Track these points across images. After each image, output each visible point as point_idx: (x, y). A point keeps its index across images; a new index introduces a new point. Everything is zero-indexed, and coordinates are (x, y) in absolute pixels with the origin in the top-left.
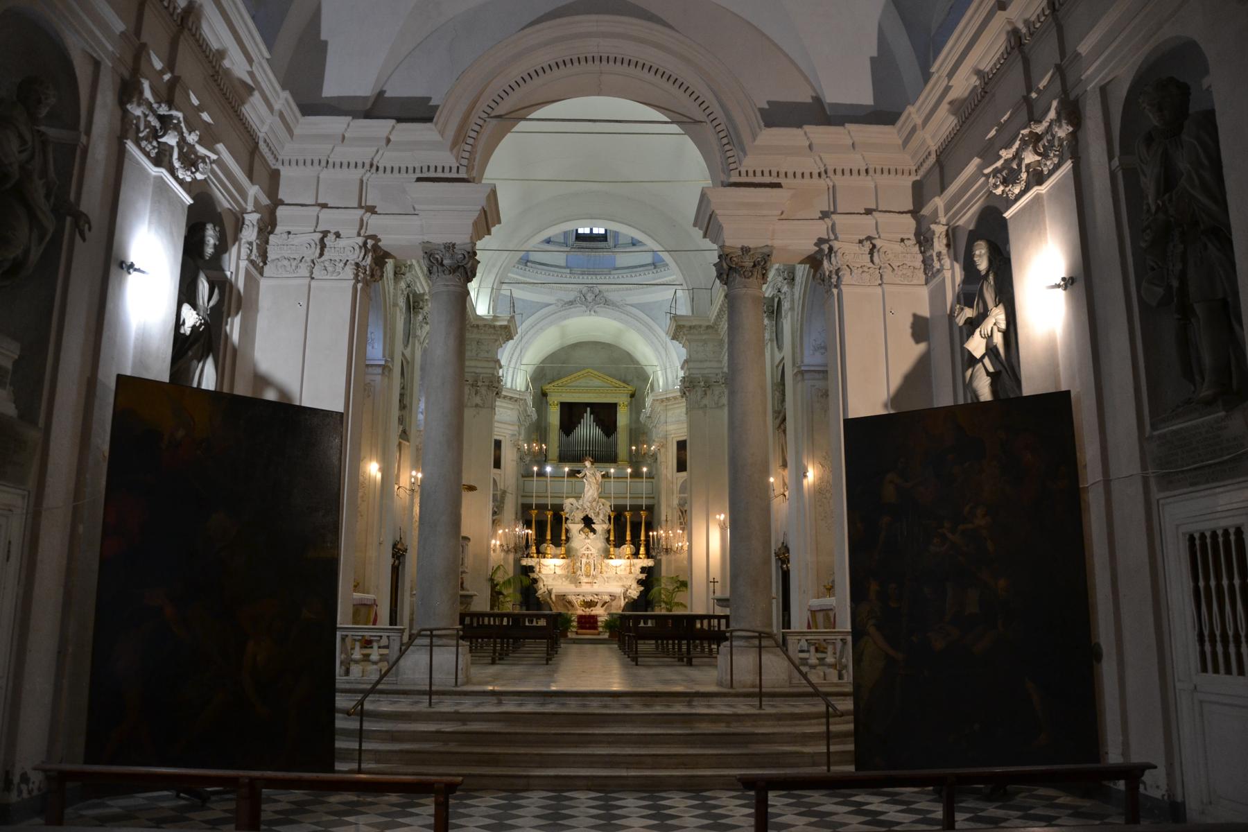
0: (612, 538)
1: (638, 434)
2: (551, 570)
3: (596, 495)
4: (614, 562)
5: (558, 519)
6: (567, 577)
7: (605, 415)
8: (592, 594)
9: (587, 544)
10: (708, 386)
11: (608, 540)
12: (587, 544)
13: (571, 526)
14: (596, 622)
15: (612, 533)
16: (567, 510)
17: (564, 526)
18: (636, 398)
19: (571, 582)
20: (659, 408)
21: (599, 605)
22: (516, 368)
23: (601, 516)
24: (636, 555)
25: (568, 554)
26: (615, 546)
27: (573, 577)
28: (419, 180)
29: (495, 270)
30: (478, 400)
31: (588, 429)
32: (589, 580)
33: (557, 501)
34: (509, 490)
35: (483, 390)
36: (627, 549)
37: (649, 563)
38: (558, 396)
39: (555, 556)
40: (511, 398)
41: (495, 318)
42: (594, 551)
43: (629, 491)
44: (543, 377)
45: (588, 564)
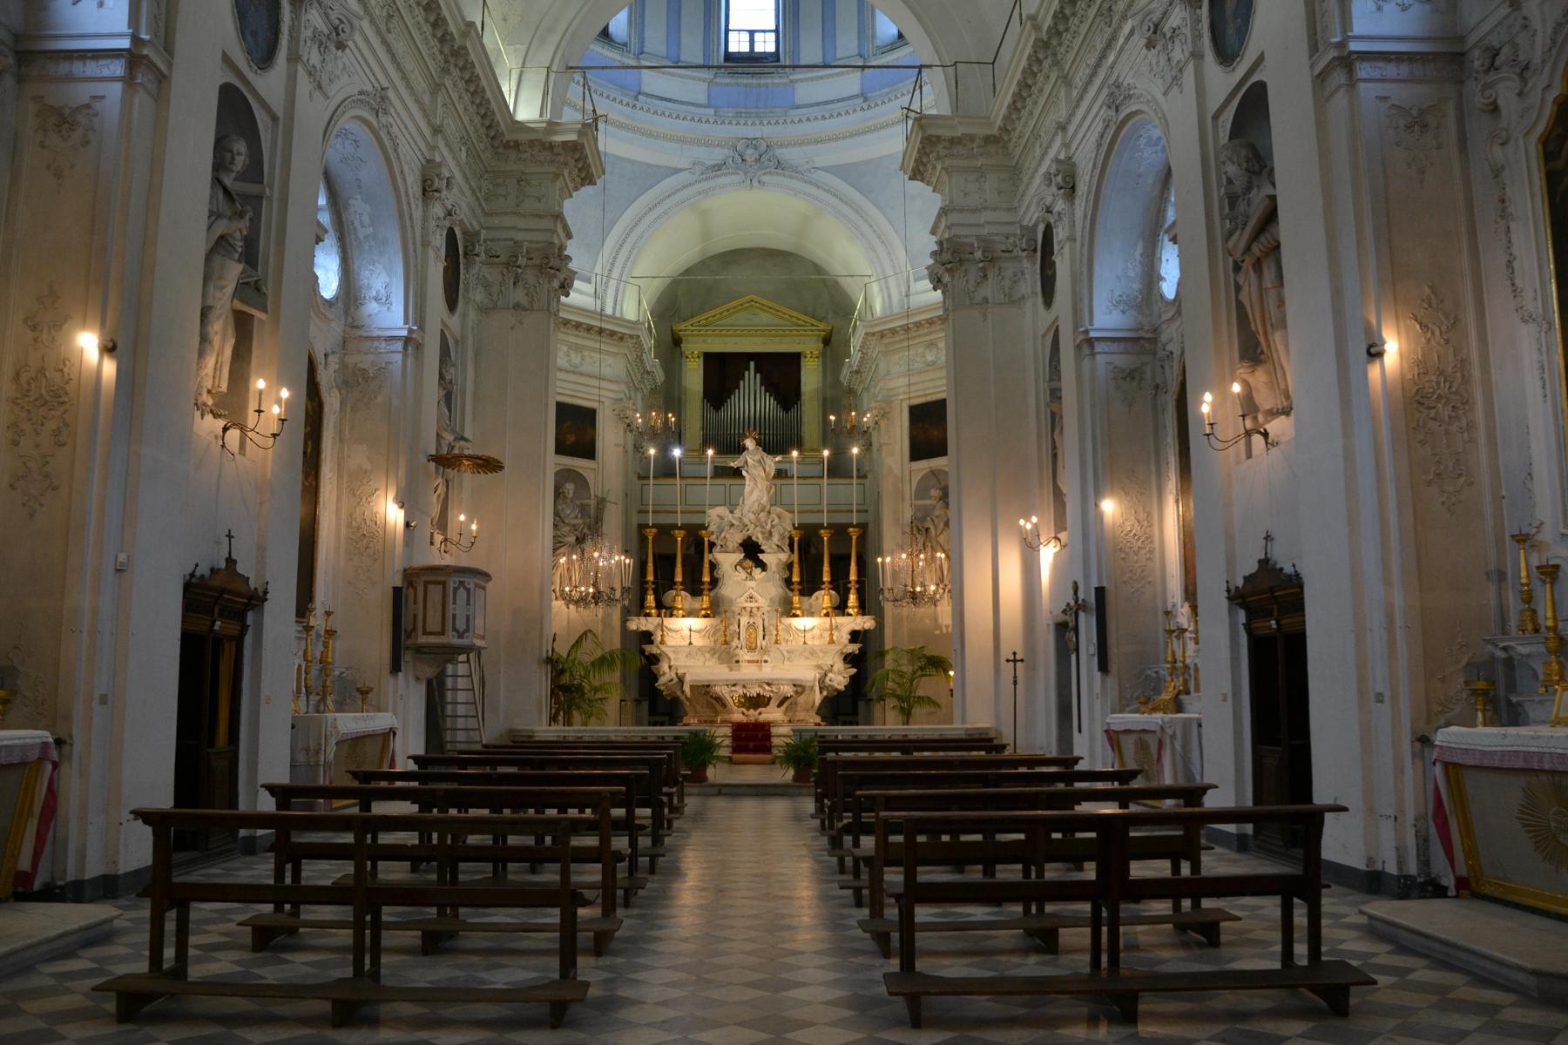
0: (796, 578)
1: (839, 397)
2: (683, 634)
3: (765, 500)
4: (801, 623)
5: (698, 544)
6: (713, 651)
7: (780, 373)
8: (760, 683)
9: (750, 590)
10: (991, 259)
11: (788, 582)
12: (750, 590)
13: (719, 556)
14: (768, 737)
15: (796, 569)
16: (712, 528)
17: (707, 557)
18: (833, 345)
19: (721, 660)
20: (875, 349)
21: (773, 704)
22: (618, 273)
23: (776, 539)
24: (841, 608)
25: (715, 610)
26: (802, 593)
27: (724, 650)
29: (554, 39)
30: (519, 295)
31: (751, 398)
33: (694, 519)
34: (611, 498)
35: (530, 277)
36: (824, 598)
37: (867, 623)
38: (697, 345)
39: (690, 613)
40: (612, 334)
41: (552, 127)
42: (762, 602)
43: (827, 501)
45: (751, 626)
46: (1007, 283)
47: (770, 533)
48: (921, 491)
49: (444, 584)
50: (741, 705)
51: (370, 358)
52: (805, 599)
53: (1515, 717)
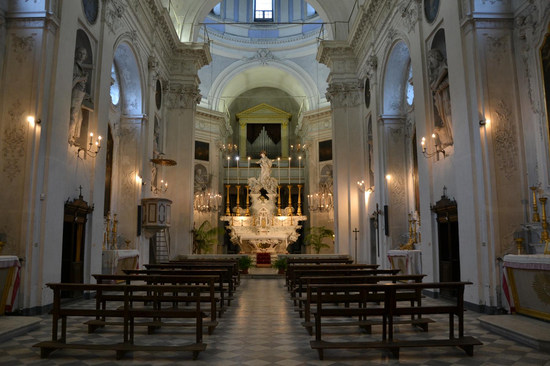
0: (279, 203)
1: (294, 139)
2: (240, 222)
3: (268, 175)
4: (281, 218)
5: (245, 190)
6: (250, 228)
7: (274, 130)
8: (267, 239)
9: (263, 207)
10: (347, 91)
11: (276, 204)
12: (263, 207)
13: (252, 195)
14: (269, 258)
15: (279, 199)
16: (250, 185)
17: (248, 195)
18: (292, 121)
19: (253, 231)
20: (307, 122)
21: (271, 246)
22: (217, 96)
23: (272, 189)
24: (295, 213)
25: (251, 214)
26: (281, 208)
27: (254, 227)
29: (194, 14)
30: (182, 103)
31: (264, 139)
33: (243, 182)
34: (214, 174)
35: (186, 97)
36: (289, 209)
37: (304, 218)
38: (245, 121)
39: (242, 215)
40: (215, 117)
41: (194, 44)
42: (267, 211)
43: (290, 175)
44: (238, 106)
45: (263, 219)
46: (353, 99)
47: (270, 187)
48: (323, 172)
49: (156, 204)
50: (260, 247)
51: (130, 125)
52: (282, 210)
53: (531, 251)
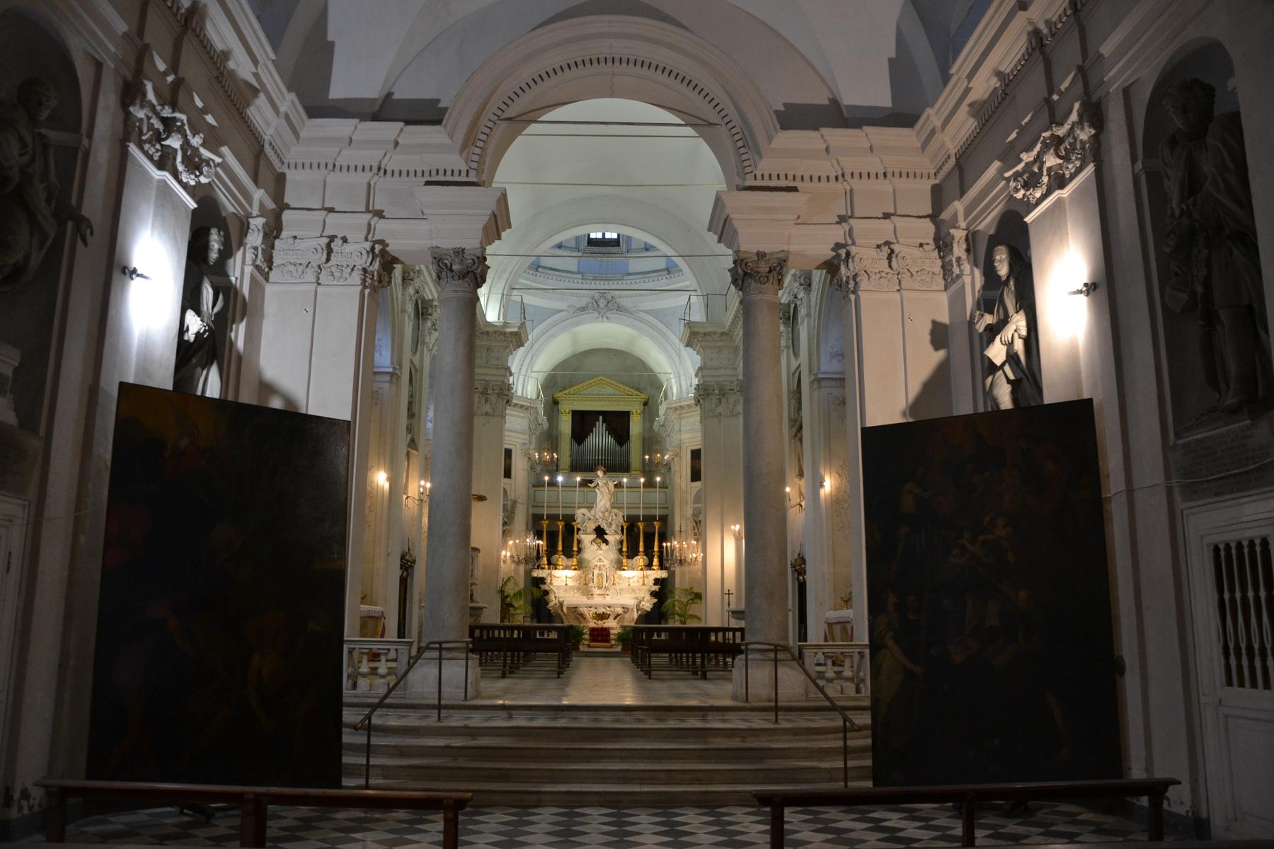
0: (625, 549)
1: (652, 442)
2: (562, 581)
3: (608, 505)
4: (627, 574)
5: (570, 530)
6: (578, 589)
7: (618, 423)
8: (604, 606)
9: (599, 556)
10: (723, 394)
11: (620, 551)
12: (599, 556)
13: (583, 537)
14: (609, 634)
15: (625, 544)
16: (579, 520)
17: (576, 537)
18: (649, 406)
19: (583, 594)
20: (673, 416)
21: (612, 618)
22: (527, 376)
23: (614, 527)
24: (649, 566)
25: (580, 566)
26: (628, 557)
27: (585, 588)
28: (428, 183)
29: (505, 276)
30: (487, 408)
31: (600, 438)
32: (602, 592)
33: (568, 512)
34: (520, 500)
35: (493, 398)
36: (640, 560)
37: (663, 574)
38: (570, 404)
39: (566, 568)
40: (522, 406)
41: (506, 324)
42: (606, 562)
43: (642, 501)
44: (554, 384)
45: (600, 575)
